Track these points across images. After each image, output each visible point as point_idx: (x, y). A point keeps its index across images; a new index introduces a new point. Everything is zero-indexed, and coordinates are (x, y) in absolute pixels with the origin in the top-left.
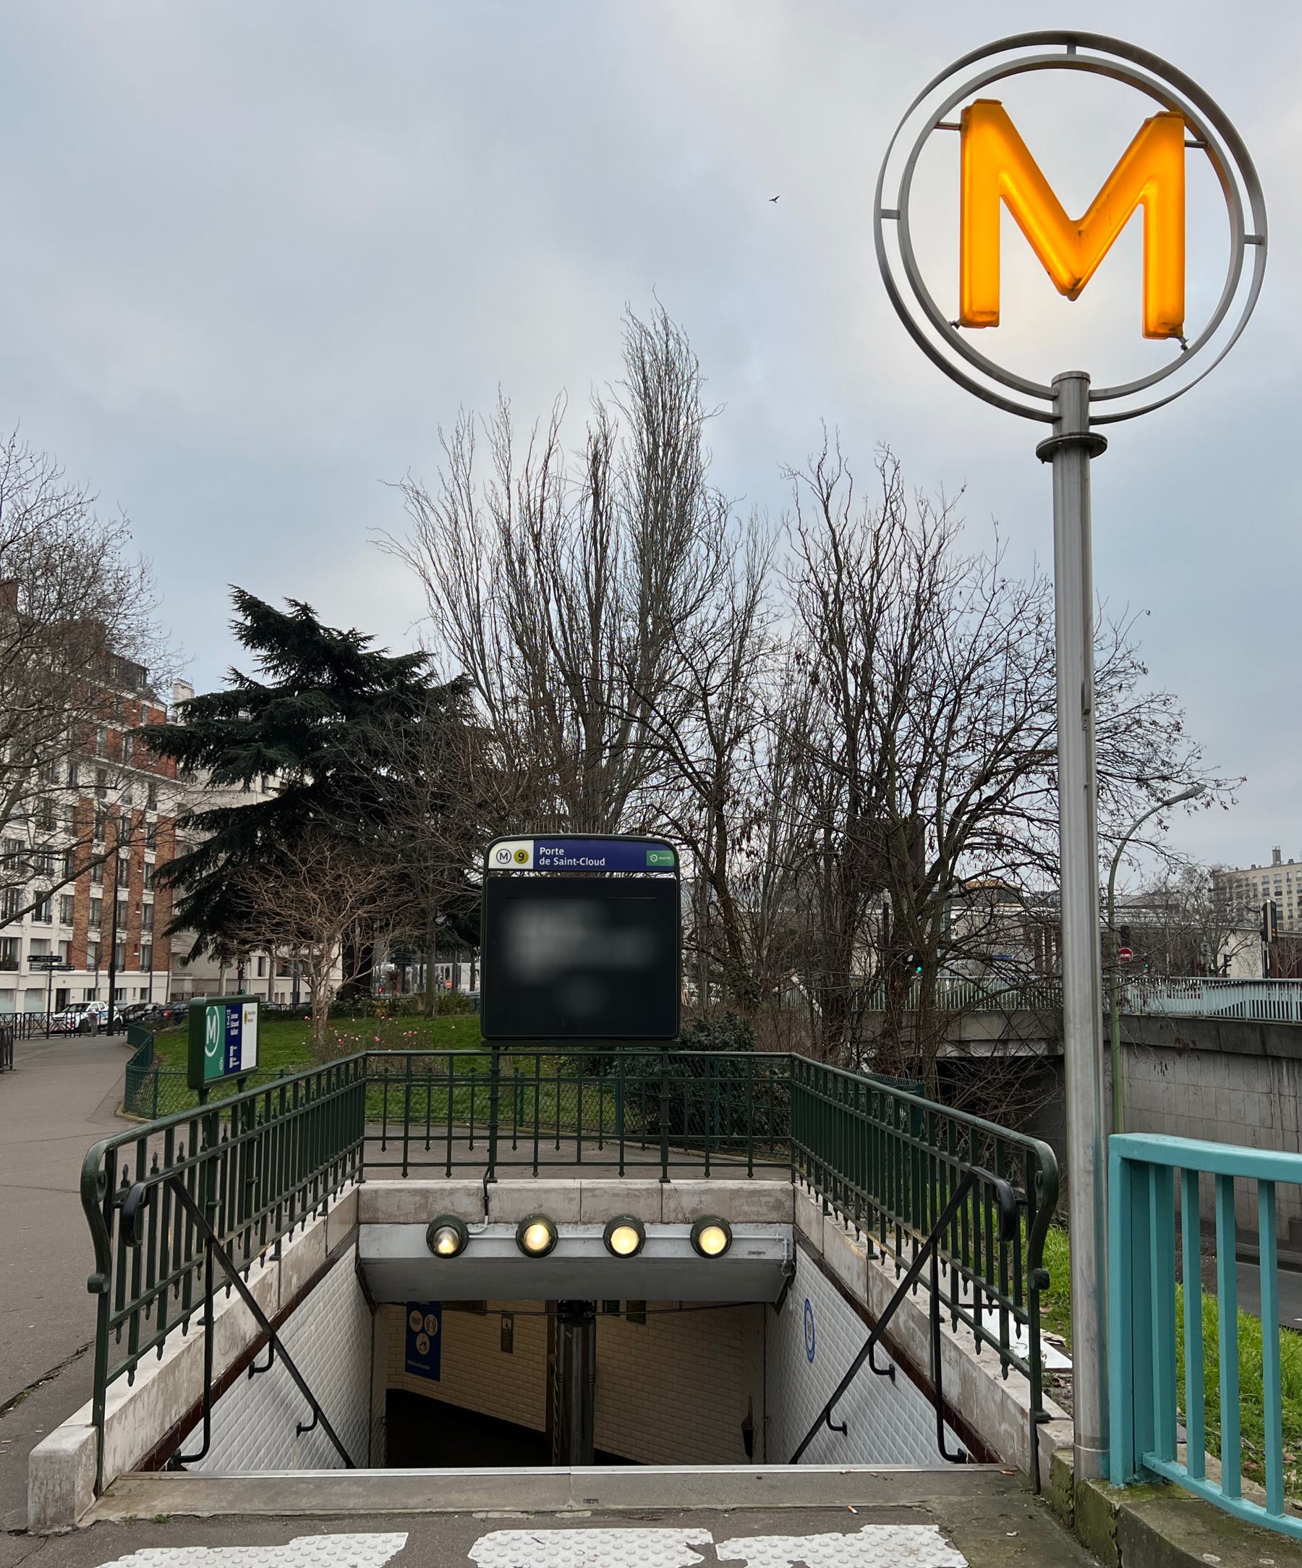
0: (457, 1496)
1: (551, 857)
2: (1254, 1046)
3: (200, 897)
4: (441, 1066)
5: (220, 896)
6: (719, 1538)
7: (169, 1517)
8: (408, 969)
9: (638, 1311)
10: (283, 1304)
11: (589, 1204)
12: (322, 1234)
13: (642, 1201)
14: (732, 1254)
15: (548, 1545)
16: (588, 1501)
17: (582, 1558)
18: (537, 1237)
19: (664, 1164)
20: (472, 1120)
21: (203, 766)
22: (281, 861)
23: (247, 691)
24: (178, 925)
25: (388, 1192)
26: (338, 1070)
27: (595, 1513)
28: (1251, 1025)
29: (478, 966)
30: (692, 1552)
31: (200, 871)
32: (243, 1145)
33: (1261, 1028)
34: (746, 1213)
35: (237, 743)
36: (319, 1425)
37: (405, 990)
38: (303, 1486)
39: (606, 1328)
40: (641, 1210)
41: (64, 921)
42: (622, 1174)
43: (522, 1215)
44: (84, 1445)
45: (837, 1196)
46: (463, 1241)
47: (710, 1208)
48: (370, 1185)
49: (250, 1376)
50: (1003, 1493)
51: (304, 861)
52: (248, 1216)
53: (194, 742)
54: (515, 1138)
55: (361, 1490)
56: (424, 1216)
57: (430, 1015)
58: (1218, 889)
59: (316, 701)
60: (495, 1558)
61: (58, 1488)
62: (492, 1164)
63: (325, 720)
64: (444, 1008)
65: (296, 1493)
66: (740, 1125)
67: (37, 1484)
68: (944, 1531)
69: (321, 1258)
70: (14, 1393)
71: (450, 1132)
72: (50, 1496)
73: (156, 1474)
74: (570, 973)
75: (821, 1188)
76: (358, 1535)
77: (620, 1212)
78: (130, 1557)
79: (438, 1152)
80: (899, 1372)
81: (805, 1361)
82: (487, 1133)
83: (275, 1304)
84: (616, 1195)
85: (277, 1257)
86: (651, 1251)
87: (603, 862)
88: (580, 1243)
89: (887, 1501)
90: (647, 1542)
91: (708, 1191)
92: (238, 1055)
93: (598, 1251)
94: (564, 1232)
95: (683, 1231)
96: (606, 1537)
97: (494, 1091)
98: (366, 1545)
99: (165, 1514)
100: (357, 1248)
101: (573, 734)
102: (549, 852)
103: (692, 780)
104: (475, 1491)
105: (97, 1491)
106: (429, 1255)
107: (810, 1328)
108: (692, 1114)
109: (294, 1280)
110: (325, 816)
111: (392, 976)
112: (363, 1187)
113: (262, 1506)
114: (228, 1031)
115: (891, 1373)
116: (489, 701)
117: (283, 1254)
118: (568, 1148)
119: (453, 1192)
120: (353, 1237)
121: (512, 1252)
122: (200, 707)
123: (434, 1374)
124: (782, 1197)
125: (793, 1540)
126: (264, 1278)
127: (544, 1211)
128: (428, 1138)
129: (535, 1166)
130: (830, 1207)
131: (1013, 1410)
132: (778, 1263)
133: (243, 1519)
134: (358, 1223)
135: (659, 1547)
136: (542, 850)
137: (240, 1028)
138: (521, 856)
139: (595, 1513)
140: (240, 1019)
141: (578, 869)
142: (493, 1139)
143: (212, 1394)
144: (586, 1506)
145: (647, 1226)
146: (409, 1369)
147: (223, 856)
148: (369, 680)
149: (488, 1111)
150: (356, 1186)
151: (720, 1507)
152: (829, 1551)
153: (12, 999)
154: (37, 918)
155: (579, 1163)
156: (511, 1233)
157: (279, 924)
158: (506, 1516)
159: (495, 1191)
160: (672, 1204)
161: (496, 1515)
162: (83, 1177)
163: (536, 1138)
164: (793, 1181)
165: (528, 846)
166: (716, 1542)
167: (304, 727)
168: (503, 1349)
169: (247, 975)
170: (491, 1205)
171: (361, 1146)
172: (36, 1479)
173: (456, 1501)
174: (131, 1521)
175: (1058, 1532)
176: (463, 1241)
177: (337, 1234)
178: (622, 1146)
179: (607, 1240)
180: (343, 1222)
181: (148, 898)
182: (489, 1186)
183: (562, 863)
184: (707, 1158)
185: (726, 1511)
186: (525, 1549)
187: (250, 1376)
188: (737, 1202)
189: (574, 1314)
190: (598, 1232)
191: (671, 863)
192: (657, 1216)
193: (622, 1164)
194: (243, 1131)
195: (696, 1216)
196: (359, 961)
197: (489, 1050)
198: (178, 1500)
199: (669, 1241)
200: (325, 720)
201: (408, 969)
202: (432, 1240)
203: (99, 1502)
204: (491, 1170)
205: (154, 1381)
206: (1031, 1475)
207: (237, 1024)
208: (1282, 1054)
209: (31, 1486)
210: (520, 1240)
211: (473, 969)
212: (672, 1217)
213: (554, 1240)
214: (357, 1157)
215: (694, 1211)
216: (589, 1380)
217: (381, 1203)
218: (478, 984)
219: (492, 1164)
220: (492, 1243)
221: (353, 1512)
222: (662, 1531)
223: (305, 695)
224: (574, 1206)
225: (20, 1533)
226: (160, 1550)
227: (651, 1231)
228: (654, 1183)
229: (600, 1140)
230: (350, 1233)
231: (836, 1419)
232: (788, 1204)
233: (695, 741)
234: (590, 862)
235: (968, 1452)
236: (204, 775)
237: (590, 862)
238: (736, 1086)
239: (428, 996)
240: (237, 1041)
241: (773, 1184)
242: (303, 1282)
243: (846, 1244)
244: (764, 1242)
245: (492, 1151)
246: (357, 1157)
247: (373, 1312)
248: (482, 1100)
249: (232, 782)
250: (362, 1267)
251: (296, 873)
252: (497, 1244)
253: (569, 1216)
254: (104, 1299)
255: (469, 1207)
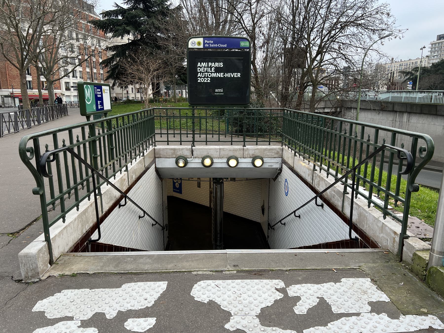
0: (186, 263)
1: (209, 44)
2: (390, 108)
3: (113, 70)
4: (177, 113)
5: (118, 69)
6: (287, 285)
7: (77, 274)
8: (170, 91)
9: (233, 179)
10: (130, 184)
11: (222, 153)
12: (143, 162)
13: (238, 152)
14: (263, 167)
15: (221, 288)
16: (234, 266)
17: (235, 295)
18: (207, 162)
19: (244, 141)
20: (187, 129)
21: (110, 32)
22: (133, 59)
23: (120, 10)
24: (108, 78)
25: (163, 149)
26: (144, 112)
27: (238, 271)
28: (391, 103)
29: (187, 91)
30: (278, 293)
31: (112, 63)
32: (108, 136)
33: (393, 104)
34: (268, 155)
35: (118, 25)
36: (146, 215)
37: (169, 96)
38: (129, 259)
39: (227, 185)
40: (237, 154)
41: (80, 78)
42: (232, 144)
43: (203, 156)
44: (40, 250)
45: (304, 152)
46: (186, 163)
47: (258, 154)
48: (158, 147)
49: (119, 207)
50: (388, 262)
51: (138, 59)
52: (113, 158)
53: (106, 25)
54: (200, 134)
55: (150, 261)
56: (174, 156)
57: (175, 102)
58: (376, 69)
59: (139, 12)
60: (201, 295)
61: (31, 266)
62: (194, 141)
63: (142, 18)
64: (179, 101)
65: (126, 262)
66: (261, 130)
67: (23, 265)
68: (374, 281)
69: (144, 169)
70: (37, 217)
71: (181, 132)
72: (29, 269)
73: (76, 254)
74: (216, 82)
75: (290, 146)
76: (149, 283)
77: (231, 155)
78: (59, 294)
79: (178, 138)
80: (325, 206)
81: (285, 196)
82: (192, 133)
83: (127, 184)
84: (230, 150)
85: (127, 170)
86: (240, 166)
87: (226, 46)
88: (220, 163)
89: (346, 266)
90: (259, 286)
91: (257, 149)
92: (102, 104)
93: (225, 166)
94: (215, 160)
95: (250, 160)
96: (243, 284)
97: (193, 120)
98: (151, 288)
99: (76, 273)
100: (155, 165)
101: (211, 19)
102: (208, 42)
103: (246, 32)
104: (192, 261)
105: (51, 262)
106: (176, 167)
107: (287, 187)
108: (248, 127)
109: (134, 177)
110: (144, 46)
111: (165, 93)
112: (156, 148)
113: (113, 269)
114: (96, 95)
115: (322, 206)
116: (187, 10)
117: (129, 169)
118: (216, 137)
119: (182, 149)
120: (154, 162)
121: (200, 166)
122: (106, 14)
123: (181, 192)
124: (279, 150)
125: (316, 286)
126: (122, 177)
127: (209, 155)
128: (174, 134)
129: (206, 142)
130: (297, 154)
131: (389, 231)
132: (277, 169)
133: (106, 274)
134: (155, 158)
135: (265, 289)
136: (206, 41)
137: (102, 95)
138: (199, 43)
139: (238, 271)
140: (101, 91)
141: (218, 48)
142: (194, 134)
143: (100, 221)
144: (234, 269)
145: (239, 159)
146: (174, 191)
147: (118, 59)
148: (153, 6)
149: (192, 127)
150: (153, 147)
151: (284, 269)
152: (331, 292)
153: (70, 98)
154: (73, 76)
155: (219, 141)
156: (200, 160)
157: (133, 76)
158: (205, 273)
159: (195, 149)
160: (246, 153)
161: (200, 273)
162: (20, 150)
163: (206, 134)
164: (282, 146)
165: (201, 40)
166: (286, 287)
167: (136, 21)
168: (198, 187)
169: (129, 92)
170: (194, 153)
171: (155, 136)
172: (22, 263)
173: (185, 266)
174: (63, 276)
175: (420, 284)
176: (186, 163)
177: (148, 162)
178: (232, 137)
179: (228, 163)
180: (149, 158)
181: (102, 72)
182: (193, 148)
183: (212, 46)
184: (257, 140)
185: (286, 271)
186: (213, 291)
187: (119, 207)
188: (266, 152)
189: (218, 181)
190: (225, 160)
191: (248, 46)
192: (242, 156)
193: (232, 141)
194: (107, 131)
195: (254, 156)
196: (156, 88)
197: (191, 108)
198: (82, 266)
199: (245, 163)
200: (142, 18)
201: (170, 91)
202: (177, 163)
203: (52, 267)
204: (193, 143)
205: (75, 220)
206: (397, 255)
207: (100, 93)
208: (398, 110)
209: (21, 265)
210: (203, 163)
211: (186, 91)
212: (247, 156)
213: (212, 163)
214: (153, 139)
215: (253, 155)
216: (222, 198)
217: (161, 152)
218: (187, 95)
219: (194, 141)
220: (195, 163)
221: (147, 271)
222: (265, 281)
223: (136, 11)
224: (218, 153)
225: (19, 281)
226: (71, 290)
227: (240, 160)
228: (241, 147)
229: (225, 135)
230: (153, 161)
231: (297, 213)
232: (281, 152)
233: (247, 20)
234: (222, 46)
235: (360, 238)
236: (110, 35)
237: (222, 46)
238: (260, 119)
239: (174, 97)
240: (101, 99)
241: (276, 147)
242: (137, 176)
243: (304, 165)
244: (273, 163)
245: (193, 137)
246: (153, 139)
247: (162, 181)
248: (190, 124)
249: (118, 37)
250: (157, 170)
251: (136, 62)
252: (196, 164)
253: (216, 156)
254: (43, 197)
255: (188, 153)
